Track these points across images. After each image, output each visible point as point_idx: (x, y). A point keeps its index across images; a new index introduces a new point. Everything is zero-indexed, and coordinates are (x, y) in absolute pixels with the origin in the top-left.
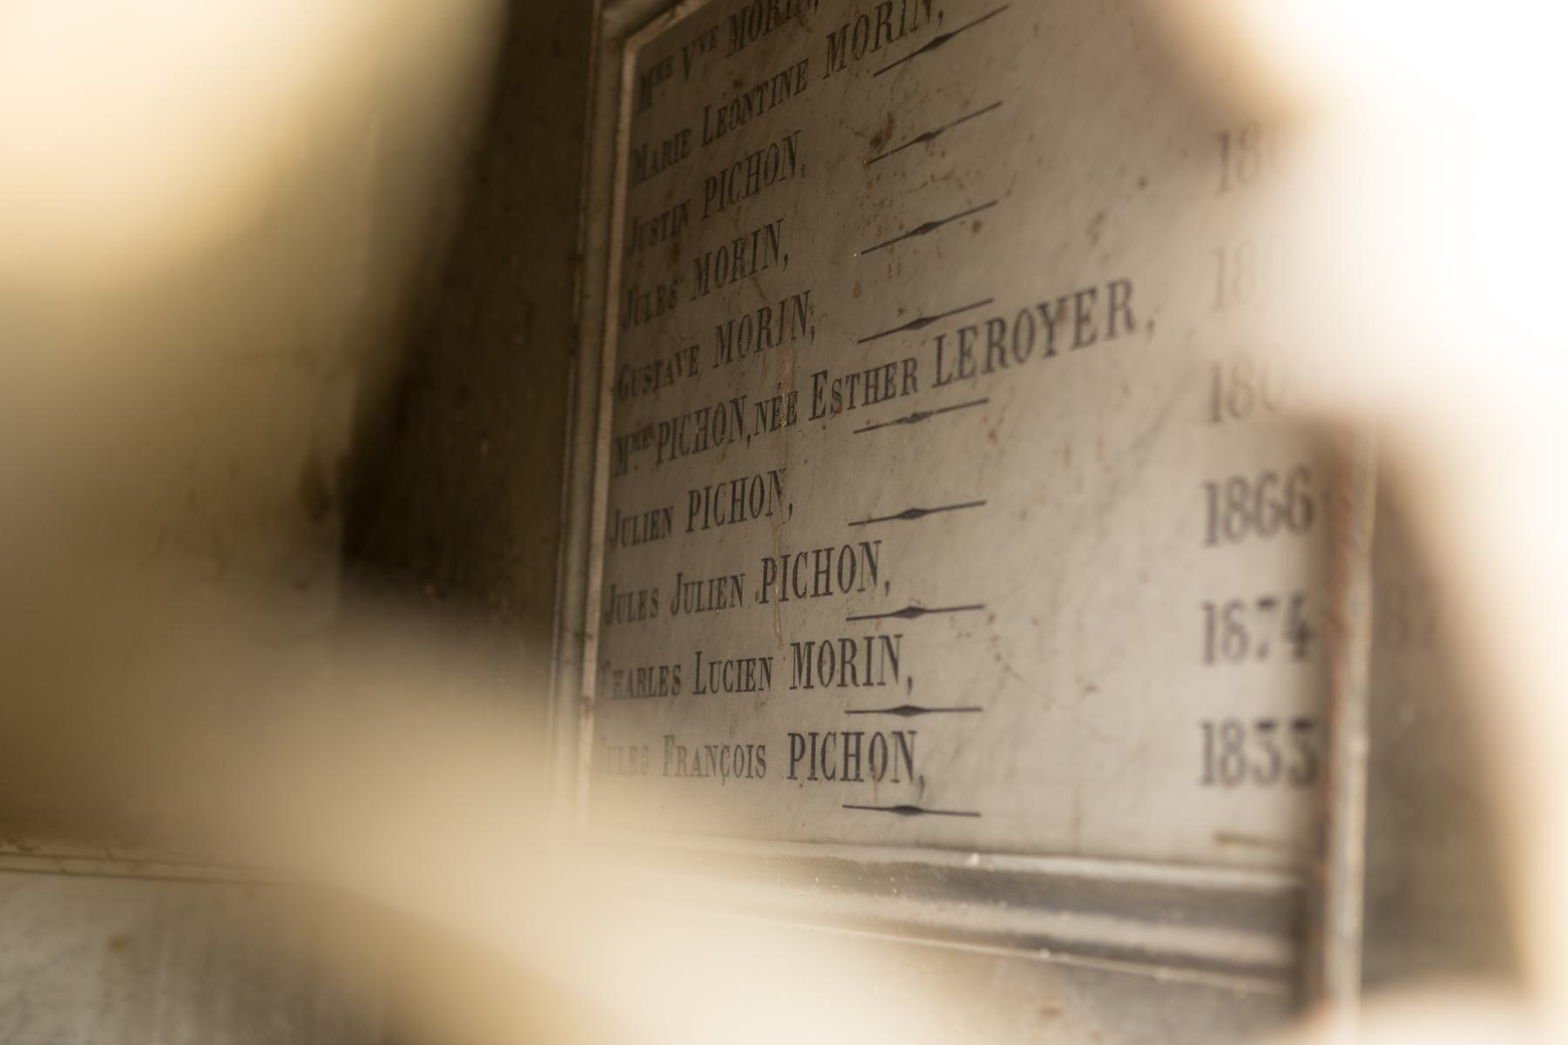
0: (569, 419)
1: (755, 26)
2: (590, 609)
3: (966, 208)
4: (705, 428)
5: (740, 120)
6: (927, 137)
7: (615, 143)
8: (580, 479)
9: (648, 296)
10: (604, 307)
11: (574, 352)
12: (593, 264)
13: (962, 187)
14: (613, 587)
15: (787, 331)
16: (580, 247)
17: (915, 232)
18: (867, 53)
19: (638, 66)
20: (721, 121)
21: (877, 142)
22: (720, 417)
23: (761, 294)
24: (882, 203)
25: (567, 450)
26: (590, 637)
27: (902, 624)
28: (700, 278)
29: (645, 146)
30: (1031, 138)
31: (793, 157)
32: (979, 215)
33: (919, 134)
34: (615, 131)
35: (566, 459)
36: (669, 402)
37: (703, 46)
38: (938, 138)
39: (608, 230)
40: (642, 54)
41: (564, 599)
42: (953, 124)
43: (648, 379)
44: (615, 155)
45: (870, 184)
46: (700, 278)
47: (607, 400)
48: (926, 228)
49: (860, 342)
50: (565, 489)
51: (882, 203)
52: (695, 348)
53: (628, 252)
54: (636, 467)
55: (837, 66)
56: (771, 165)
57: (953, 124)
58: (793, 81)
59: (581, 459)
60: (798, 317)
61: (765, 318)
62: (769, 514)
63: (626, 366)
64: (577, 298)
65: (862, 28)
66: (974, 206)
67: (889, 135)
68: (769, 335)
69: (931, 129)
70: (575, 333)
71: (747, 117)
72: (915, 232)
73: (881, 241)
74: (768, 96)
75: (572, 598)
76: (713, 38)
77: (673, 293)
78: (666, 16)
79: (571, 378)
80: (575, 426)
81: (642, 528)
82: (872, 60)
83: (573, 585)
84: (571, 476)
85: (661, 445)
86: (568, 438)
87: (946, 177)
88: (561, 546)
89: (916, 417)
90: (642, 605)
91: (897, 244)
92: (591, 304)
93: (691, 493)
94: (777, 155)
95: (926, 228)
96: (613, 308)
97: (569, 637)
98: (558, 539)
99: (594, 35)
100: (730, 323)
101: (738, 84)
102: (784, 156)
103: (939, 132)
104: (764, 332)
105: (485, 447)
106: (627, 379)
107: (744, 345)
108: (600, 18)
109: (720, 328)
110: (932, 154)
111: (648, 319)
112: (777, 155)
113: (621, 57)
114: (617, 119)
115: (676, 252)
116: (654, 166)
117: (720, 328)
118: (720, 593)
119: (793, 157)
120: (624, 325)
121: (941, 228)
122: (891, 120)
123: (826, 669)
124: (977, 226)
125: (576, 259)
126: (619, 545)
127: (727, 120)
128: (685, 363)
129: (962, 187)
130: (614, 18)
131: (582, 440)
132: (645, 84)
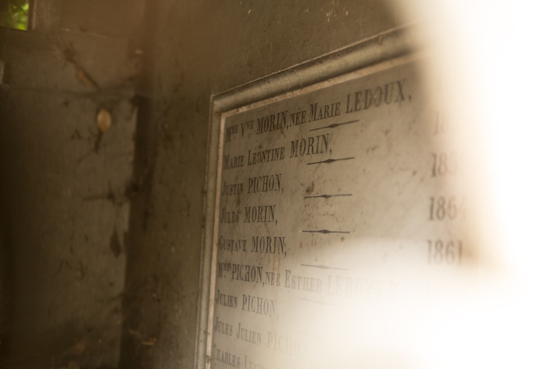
0: (202, 251)
1: (266, 127)
2: (209, 323)
3: (339, 230)
4: (249, 273)
5: (261, 161)
6: (326, 196)
7: (218, 152)
8: (206, 275)
9: (229, 213)
10: (214, 212)
11: (204, 227)
12: (210, 195)
13: (338, 221)
14: (225, 183)
15: (277, 249)
16: (205, 188)
17: (321, 231)
18: (305, 155)
19: (226, 124)
20: (254, 158)
21: (308, 191)
22: (253, 271)
23: (268, 231)
24: (310, 215)
25: (201, 263)
26: (209, 334)
27: (329, 131)
28: (247, 215)
29: (228, 156)
30: (362, 213)
31: (279, 183)
32: (344, 235)
33: (323, 194)
34: (218, 147)
35: (201, 266)
36: (236, 257)
37: (248, 126)
38: (329, 199)
39: (216, 181)
40: (227, 119)
41: (200, 318)
42: (335, 196)
43: (229, 245)
44: (218, 156)
45: (306, 206)
46: (247, 215)
47: (215, 248)
48: (325, 232)
49: (308, 164)
50: (200, 277)
51: (310, 215)
52: (245, 241)
53: (222, 194)
54: (225, 277)
55: (294, 155)
56: (272, 183)
57: (335, 196)
58: (279, 153)
59: (206, 267)
60: (280, 246)
61: (269, 241)
62: (270, 316)
63: (222, 236)
64: (204, 207)
65: (303, 143)
66: (342, 230)
67: (312, 191)
68: (270, 247)
69: (328, 193)
70: (204, 219)
71: (263, 161)
72: (321, 231)
73: (309, 230)
74: (271, 155)
75: (203, 317)
76: (252, 125)
77: (238, 217)
78: (235, 110)
79: (203, 236)
80: (204, 255)
81: (226, 300)
82: (307, 158)
83: (203, 313)
84: (203, 273)
85: (233, 272)
86: (201, 258)
87: (332, 215)
88: (199, 298)
89: (330, 161)
90: (227, 329)
91: (315, 233)
92: (210, 210)
93: (250, 179)
94: (273, 179)
95: (325, 232)
96: (217, 213)
97: (202, 332)
98: (198, 294)
99: (210, 109)
100: (257, 237)
101: (260, 147)
102: (276, 181)
103: (330, 196)
104: (269, 246)
105: (173, 249)
106: (222, 242)
107: (262, 249)
108: (213, 103)
109: (254, 237)
110: (327, 204)
111: (229, 222)
112: (273, 179)
113: (220, 120)
114: (219, 143)
115: (238, 202)
116: (231, 165)
117: (254, 237)
118: (253, 338)
119: (279, 183)
120: (221, 221)
121: (331, 234)
122: (313, 185)
123: (303, 148)
124: (343, 239)
125: (204, 192)
126: (219, 303)
127: (256, 159)
128: (242, 245)
129: (338, 221)
130: (218, 104)
131: (207, 260)
132: (229, 132)
